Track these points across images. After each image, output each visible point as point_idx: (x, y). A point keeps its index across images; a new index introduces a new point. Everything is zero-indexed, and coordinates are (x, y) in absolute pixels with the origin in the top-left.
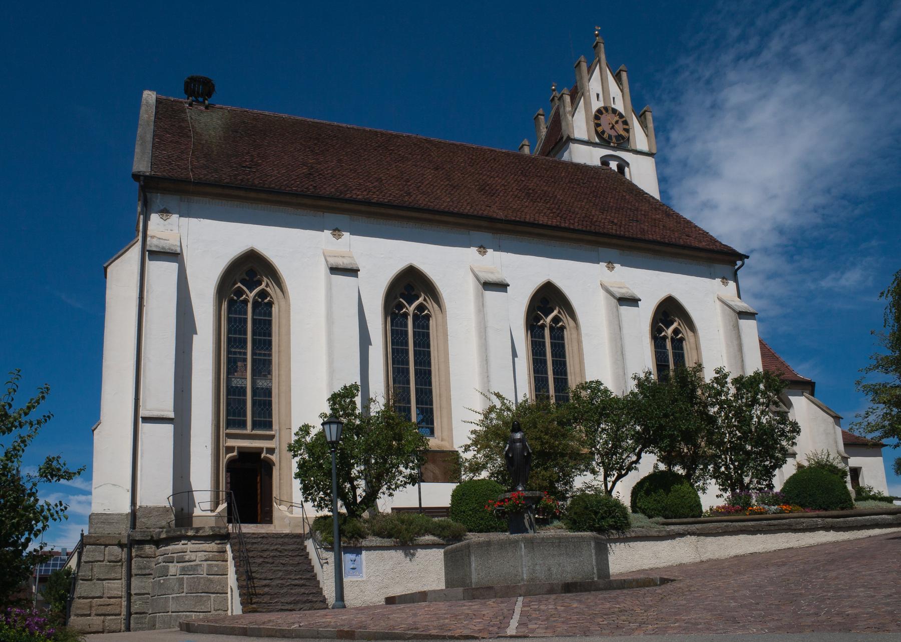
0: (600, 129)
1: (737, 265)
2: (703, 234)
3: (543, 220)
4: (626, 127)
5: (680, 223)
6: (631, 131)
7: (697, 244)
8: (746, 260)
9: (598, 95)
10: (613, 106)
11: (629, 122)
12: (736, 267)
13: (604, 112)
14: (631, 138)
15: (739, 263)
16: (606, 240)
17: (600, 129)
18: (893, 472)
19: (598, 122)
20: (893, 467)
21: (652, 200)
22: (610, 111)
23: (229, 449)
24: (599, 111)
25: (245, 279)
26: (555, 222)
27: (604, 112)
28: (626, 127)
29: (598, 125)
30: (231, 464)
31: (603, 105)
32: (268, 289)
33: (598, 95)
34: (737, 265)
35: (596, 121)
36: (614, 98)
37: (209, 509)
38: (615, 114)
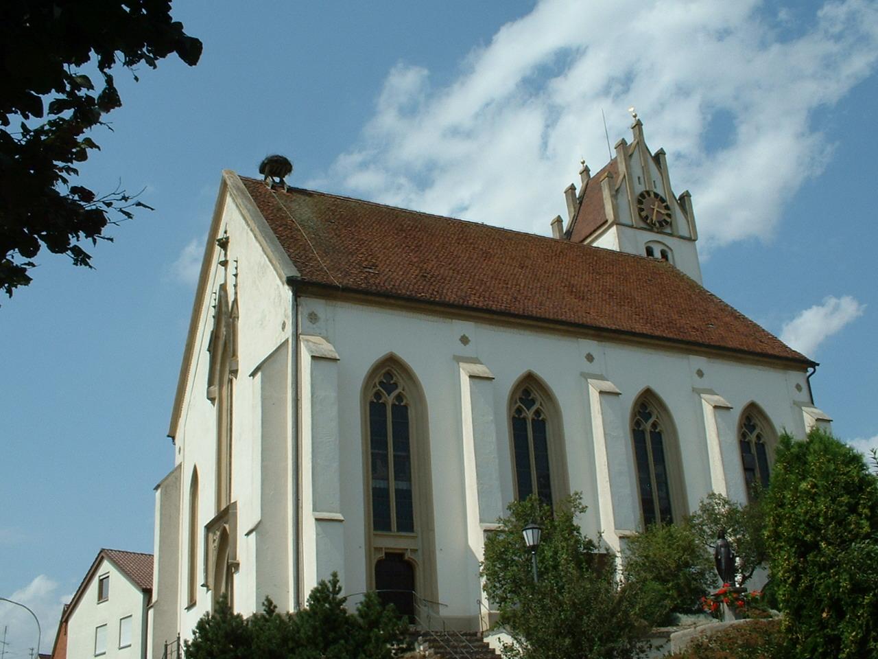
0: (643, 214)
1: (807, 371)
2: (771, 338)
3: (638, 328)
4: (669, 212)
5: (748, 326)
6: (673, 216)
7: (771, 352)
8: (817, 367)
9: (639, 178)
10: (655, 190)
11: (671, 207)
12: (808, 374)
13: (646, 196)
14: (673, 223)
15: (810, 370)
16: (696, 348)
17: (643, 214)
18: (418, 559)
19: (642, 206)
20: (360, 606)
21: (715, 299)
22: (652, 195)
23: (378, 549)
24: (642, 195)
25: (383, 382)
26: (646, 330)
27: (646, 196)
28: (669, 212)
29: (641, 210)
30: (379, 564)
31: (645, 189)
32: (404, 393)
33: (639, 178)
34: (807, 371)
35: (639, 206)
36: (654, 182)
37: (440, 606)
38: (657, 198)
